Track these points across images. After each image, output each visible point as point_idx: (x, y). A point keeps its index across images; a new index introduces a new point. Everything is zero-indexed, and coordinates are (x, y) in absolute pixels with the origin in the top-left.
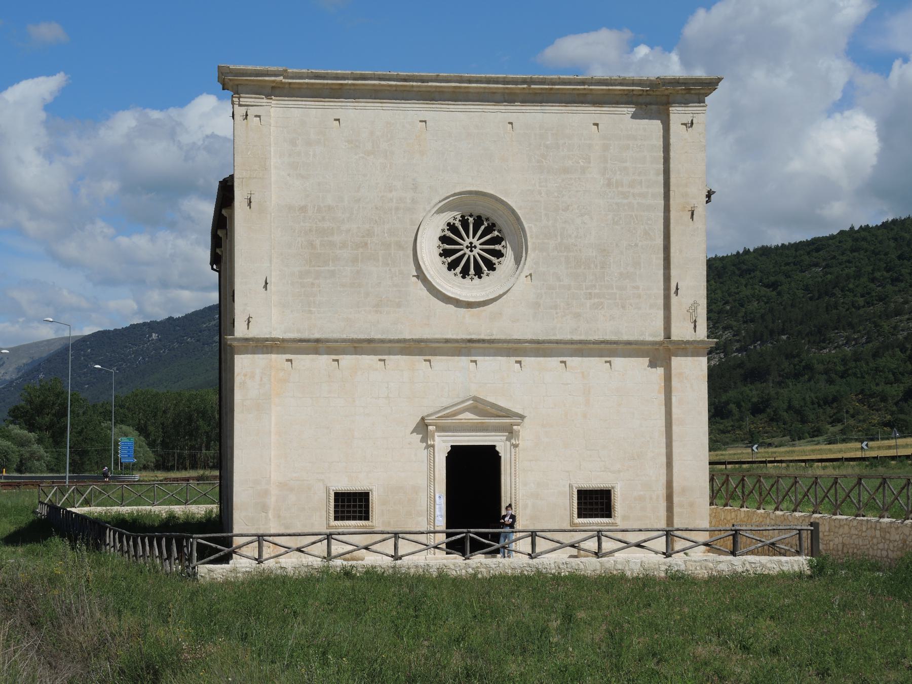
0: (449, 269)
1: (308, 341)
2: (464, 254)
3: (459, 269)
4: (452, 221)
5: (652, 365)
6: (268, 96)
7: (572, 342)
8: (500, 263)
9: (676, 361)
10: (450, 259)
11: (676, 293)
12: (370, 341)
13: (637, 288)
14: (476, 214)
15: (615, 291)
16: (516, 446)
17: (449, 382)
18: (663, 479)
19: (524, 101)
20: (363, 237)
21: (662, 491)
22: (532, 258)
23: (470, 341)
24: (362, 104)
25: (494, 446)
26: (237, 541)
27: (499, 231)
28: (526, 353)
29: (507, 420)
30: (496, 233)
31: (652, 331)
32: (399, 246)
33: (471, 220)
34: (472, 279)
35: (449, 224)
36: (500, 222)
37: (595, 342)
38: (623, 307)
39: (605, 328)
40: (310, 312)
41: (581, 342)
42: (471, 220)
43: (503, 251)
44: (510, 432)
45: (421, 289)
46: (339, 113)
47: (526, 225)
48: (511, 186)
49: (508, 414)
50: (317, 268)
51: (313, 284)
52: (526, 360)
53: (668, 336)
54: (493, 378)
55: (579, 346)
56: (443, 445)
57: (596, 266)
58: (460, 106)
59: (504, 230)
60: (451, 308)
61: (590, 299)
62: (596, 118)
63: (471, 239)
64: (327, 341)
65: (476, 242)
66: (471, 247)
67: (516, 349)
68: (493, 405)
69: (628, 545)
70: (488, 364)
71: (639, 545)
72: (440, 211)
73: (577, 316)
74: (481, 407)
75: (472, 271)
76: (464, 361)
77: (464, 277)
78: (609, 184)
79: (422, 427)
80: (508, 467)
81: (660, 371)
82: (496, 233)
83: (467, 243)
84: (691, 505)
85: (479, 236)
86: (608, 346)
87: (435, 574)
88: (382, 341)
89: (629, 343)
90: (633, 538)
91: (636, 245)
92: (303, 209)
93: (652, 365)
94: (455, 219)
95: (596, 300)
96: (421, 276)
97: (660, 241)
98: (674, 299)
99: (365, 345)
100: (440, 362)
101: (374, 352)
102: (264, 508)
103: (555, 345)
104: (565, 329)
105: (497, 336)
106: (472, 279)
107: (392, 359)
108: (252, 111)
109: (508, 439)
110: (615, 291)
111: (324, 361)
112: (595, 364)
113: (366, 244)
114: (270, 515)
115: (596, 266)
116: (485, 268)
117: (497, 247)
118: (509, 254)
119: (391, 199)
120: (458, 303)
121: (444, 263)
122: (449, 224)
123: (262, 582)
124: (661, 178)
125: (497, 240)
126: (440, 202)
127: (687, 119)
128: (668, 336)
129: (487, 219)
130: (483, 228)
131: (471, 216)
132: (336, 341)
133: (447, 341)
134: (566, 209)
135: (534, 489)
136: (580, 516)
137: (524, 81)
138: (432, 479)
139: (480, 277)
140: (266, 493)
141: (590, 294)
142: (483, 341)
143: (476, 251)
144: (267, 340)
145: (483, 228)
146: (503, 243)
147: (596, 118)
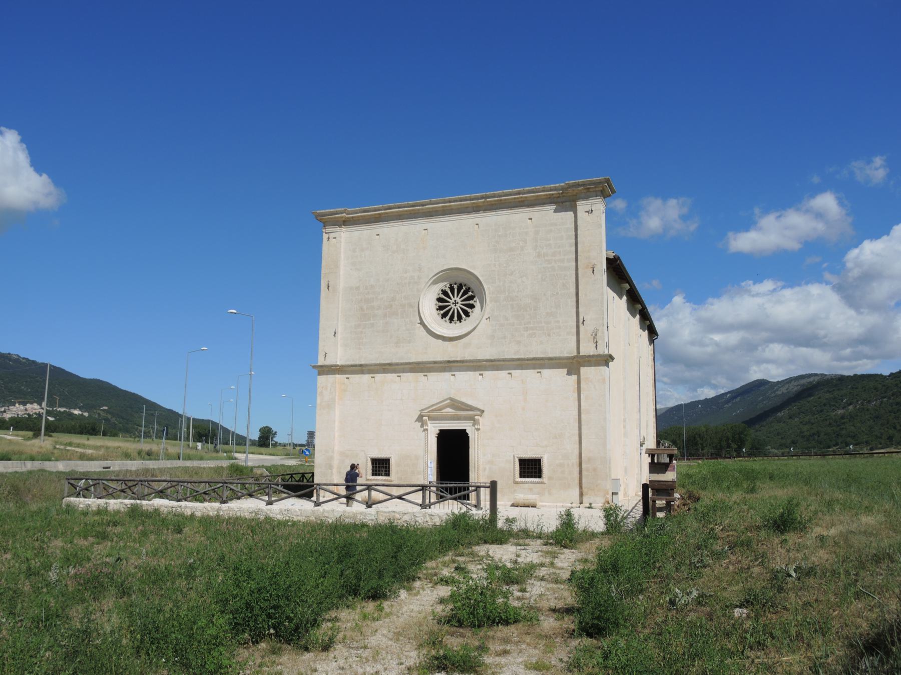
1: (355, 366)
3: (448, 317)
4: (444, 288)
5: (569, 373)
6: (340, 226)
7: (513, 360)
9: (583, 370)
11: (583, 323)
12: (390, 364)
13: (558, 322)
14: (458, 282)
16: (478, 429)
17: (439, 387)
18: (577, 452)
19: (485, 210)
21: (576, 460)
22: (489, 305)
23: (449, 362)
24: (392, 224)
25: (888, 235)
26: (358, 488)
28: (486, 368)
29: (472, 412)
30: (470, 293)
31: (567, 349)
32: (411, 306)
33: (455, 286)
36: (472, 287)
37: (528, 359)
38: (549, 335)
39: (536, 350)
41: (519, 360)
42: (455, 286)
44: (475, 423)
46: (379, 231)
47: (485, 286)
48: (477, 264)
49: (471, 408)
52: (486, 373)
53: (578, 352)
54: (462, 386)
55: (518, 362)
58: (447, 218)
62: (530, 215)
64: (367, 365)
66: (456, 303)
67: (479, 366)
68: (462, 403)
69: (392, 497)
70: (464, 377)
71: (400, 498)
72: (435, 282)
73: (519, 342)
74: (456, 404)
76: (447, 375)
78: (539, 256)
79: (420, 418)
81: (575, 377)
82: (470, 293)
84: (595, 470)
85: (460, 296)
86: (538, 362)
87: (262, 518)
88: (397, 364)
89: (551, 359)
90: (396, 492)
91: (557, 293)
92: (358, 288)
93: (569, 373)
96: (422, 323)
97: (573, 290)
98: (582, 328)
99: (387, 367)
100: (433, 377)
101: (394, 372)
102: (331, 467)
103: (502, 363)
104: (510, 352)
105: (468, 357)
107: (405, 376)
108: (332, 235)
109: (474, 425)
111: (366, 377)
112: (530, 374)
114: (335, 470)
118: (478, 305)
120: (451, 339)
123: (237, 518)
124: (573, 248)
125: (472, 298)
127: (588, 208)
128: (578, 352)
132: (371, 365)
133: (435, 362)
134: (512, 274)
135: (487, 460)
137: (482, 197)
138: (426, 451)
140: (332, 458)
142: (457, 361)
143: (453, 306)
144: (332, 366)
147: (530, 215)
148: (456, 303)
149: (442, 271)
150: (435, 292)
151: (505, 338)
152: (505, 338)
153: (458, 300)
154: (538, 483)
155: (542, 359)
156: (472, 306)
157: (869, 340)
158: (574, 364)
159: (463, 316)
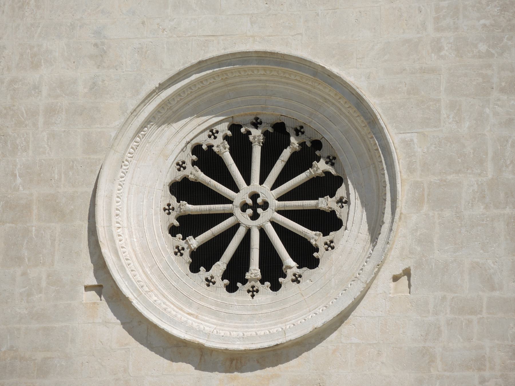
0: (194, 269)
2: (236, 227)
3: (220, 267)
4: (204, 140)
8: (181, 166)
10: (195, 242)
22: (408, 221)
27: (331, 160)
30: (321, 166)
33: (256, 135)
34: (253, 292)
35: (197, 149)
36: (332, 136)
42: (256, 135)
43: (341, 213)
45: (106, 323)
47: (394, 137)
59: (342, 157)
60: (186, 369)
65: (267, 193)
66: (255, 206)
72: (167, 114)
75: (254, 270)
77: (231, 288)
82: (321, 166)
94: (213, 134)
96: (106, 287)
106: (253, 292)
116: (288, 261)
117: (325, 203)
118: (355, 219)
121: (179, 251)
122: (197, 149)
125: (328, 185)
126: (162, 87)
129: (298, 131)
130: (286, 154)
131: (256, 124)
139: (276, 287)
145: (286, 154)
146: (341, 192)
148: (255, 206)
149: (200, 66)
150: (167, 152)
153: (267, 193)
156: (329, 223)
159: (288, 261)
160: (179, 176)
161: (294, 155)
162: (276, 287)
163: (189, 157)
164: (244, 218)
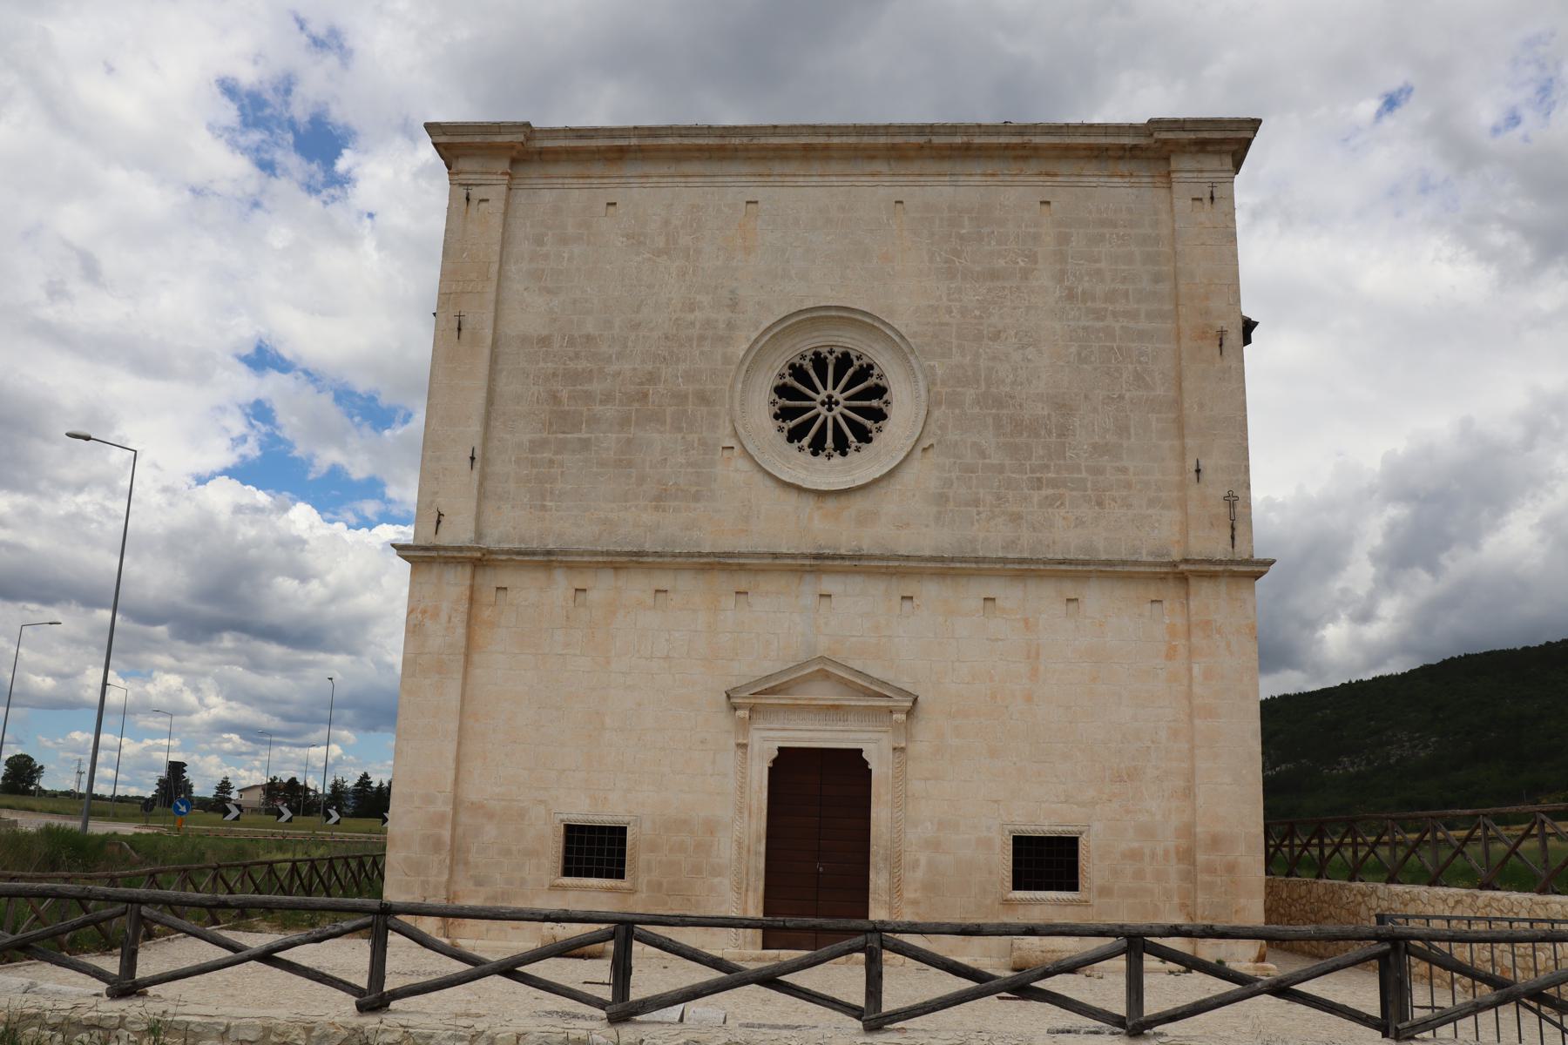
13: (1124, 470)
15: (1084, 475)
17: (777, 628)
20: (641, 384)
23: (817, 557)
25: (860, 751)
34: (829, 456)
38: (1100, 504)
40: (543, 508)
46: (615, 195)
50: (561, 436)
51: (551, 462)
56: (768, 740)
57: (1050, 433)
61: (1039, 488)
62: (899, 193)
63: (842, 402)
69: (479, 969)
71: (509, 970)
73: (1016, 518)
75: (875, 403)
77: (815, 454)
78: (1071, 296)
80: (852, 735)
83: (837, 395)
85: (831, 396)
91: (1121, 397)
92: (545, 341)
95: (1050, 491)
104: (992, 537)
110: (1084, 475)
111: (561, 586)
113: (646, 395)
115: (1050, 433)
116: (851, 438)
119: (692, 324)
121: (781, 429)
122: (792, 366)
134: (996, 336)
136: (1016, 887)
139: (844, 454)
141: (1039, 479)
145: (850, 371)
148: (830, 403)
150: (766, 382)
151: (976, 502)
152: (976, 502)
154: (1070, 903)
155: (1085, 563)
157: (756, 890)
158: (1181, 574)
160: (781, 382)
161: (855, 373)
162: (844, 454)
163: (787, 372)
164: (823, 411)
